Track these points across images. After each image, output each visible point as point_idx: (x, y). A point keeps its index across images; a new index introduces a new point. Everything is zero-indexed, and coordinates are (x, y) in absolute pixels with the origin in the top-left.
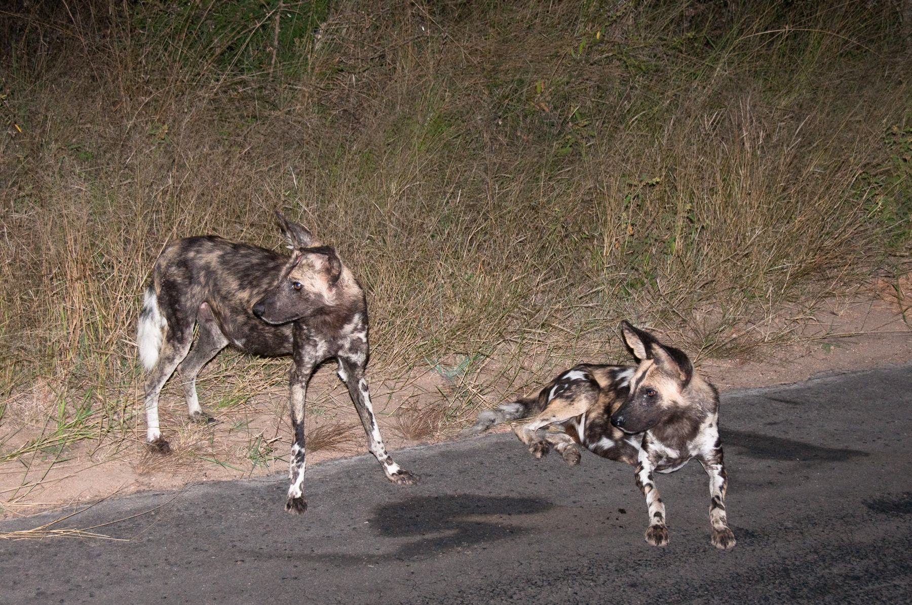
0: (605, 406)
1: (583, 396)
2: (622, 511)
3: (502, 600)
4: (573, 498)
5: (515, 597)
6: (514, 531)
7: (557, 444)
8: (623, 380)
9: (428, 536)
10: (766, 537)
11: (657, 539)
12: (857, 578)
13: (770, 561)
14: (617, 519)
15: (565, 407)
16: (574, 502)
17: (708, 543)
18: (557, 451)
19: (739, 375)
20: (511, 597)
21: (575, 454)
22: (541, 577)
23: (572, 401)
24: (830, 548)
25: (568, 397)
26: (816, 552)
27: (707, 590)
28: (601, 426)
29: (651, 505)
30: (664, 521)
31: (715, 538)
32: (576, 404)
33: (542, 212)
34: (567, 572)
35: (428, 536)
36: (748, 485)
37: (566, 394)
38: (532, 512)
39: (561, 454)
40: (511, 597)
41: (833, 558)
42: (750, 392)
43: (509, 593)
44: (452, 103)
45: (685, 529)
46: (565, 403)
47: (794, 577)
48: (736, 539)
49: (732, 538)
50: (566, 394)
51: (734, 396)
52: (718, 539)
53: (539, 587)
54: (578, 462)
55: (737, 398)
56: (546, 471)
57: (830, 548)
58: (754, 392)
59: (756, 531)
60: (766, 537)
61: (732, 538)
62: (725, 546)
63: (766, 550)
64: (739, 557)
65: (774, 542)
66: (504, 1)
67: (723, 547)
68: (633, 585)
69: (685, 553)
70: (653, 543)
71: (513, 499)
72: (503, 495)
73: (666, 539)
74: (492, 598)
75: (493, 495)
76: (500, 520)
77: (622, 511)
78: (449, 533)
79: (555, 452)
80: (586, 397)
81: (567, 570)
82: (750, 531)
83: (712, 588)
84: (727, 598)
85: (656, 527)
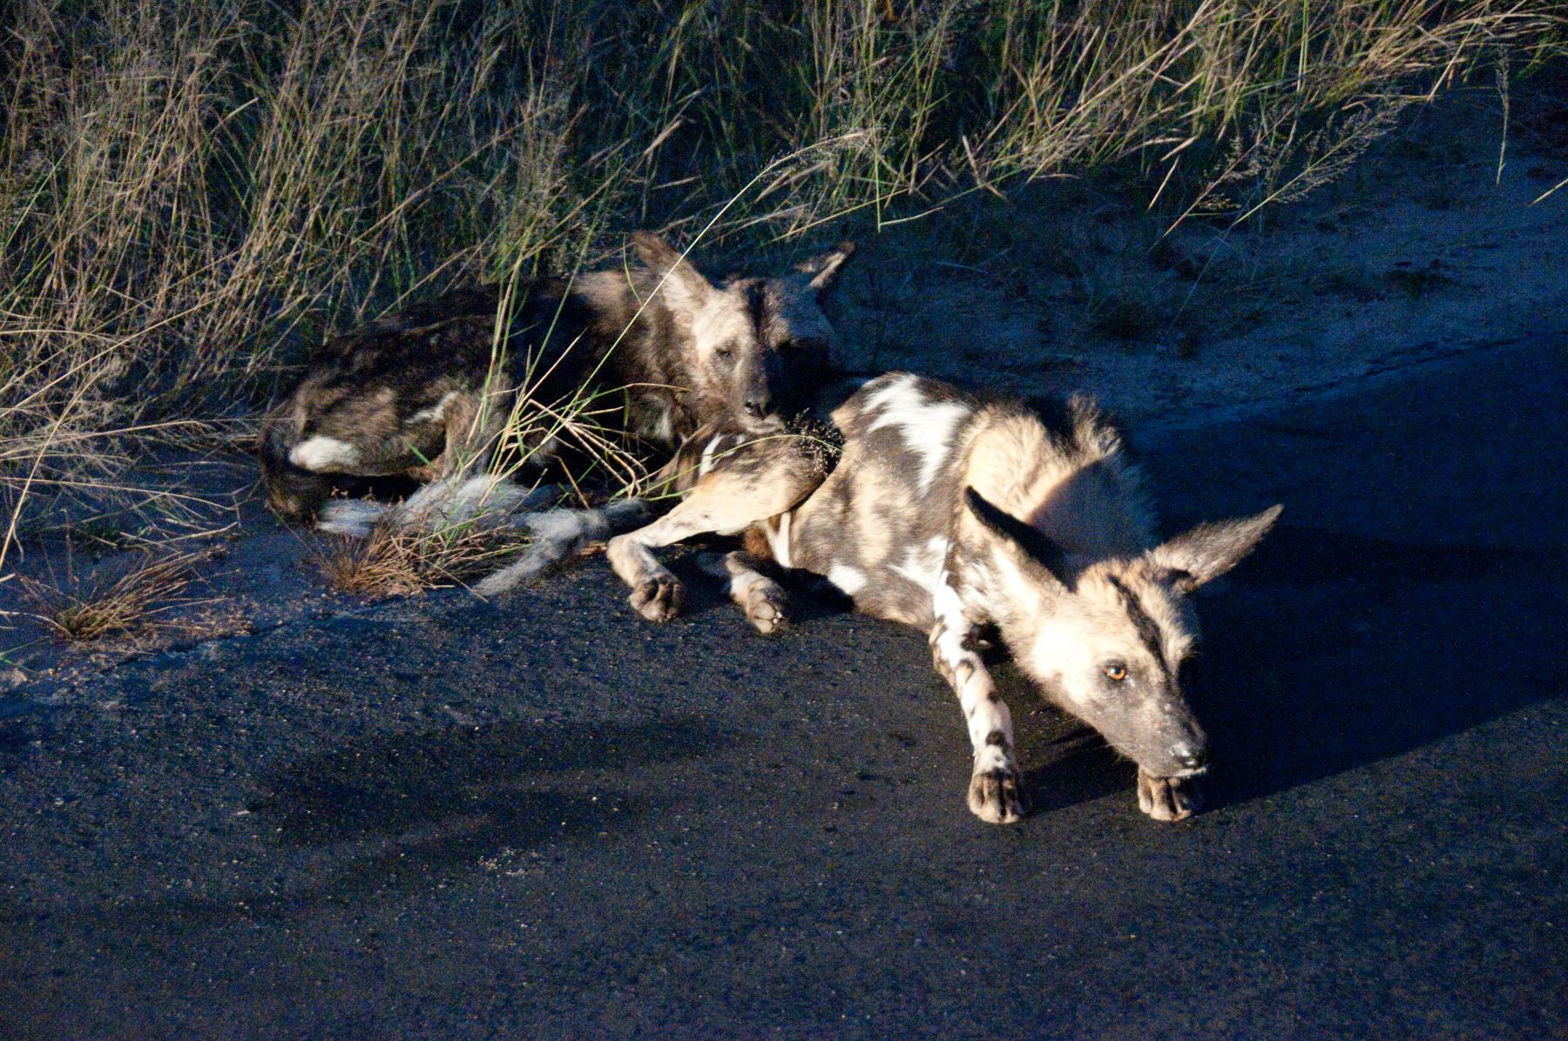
2: (908, 742)
3: (611, 989)
5: (645, 979)
6: (630, 810)
8: (880, 411)
9: (411, 838)
12: (1522, 876)
20: (634, 981)
22: (707, 924)
23: (754, 480)
24: (1449, 801)
26: (1410, 815)
27: (1134, 927)
28: (827, 534)
29: (973, 713)
33: (1149, 1011)
34: (775, 906)
35: (411, 838)
40: (634, 981)
41: (1455, 826)
43: (629, 971)
44: (12, 794)
47: (1356, 880)
53: (705, 948)
57: (1449, 801)
58: (1228, 414)
66: (220, 3)
68: (948, 929)
74: (585, 984)
77: (908, 742)
78: (462, 825)
80: (790, 473)
81: (777, 900)
83: (1150, 922)
84: (1188, 947)
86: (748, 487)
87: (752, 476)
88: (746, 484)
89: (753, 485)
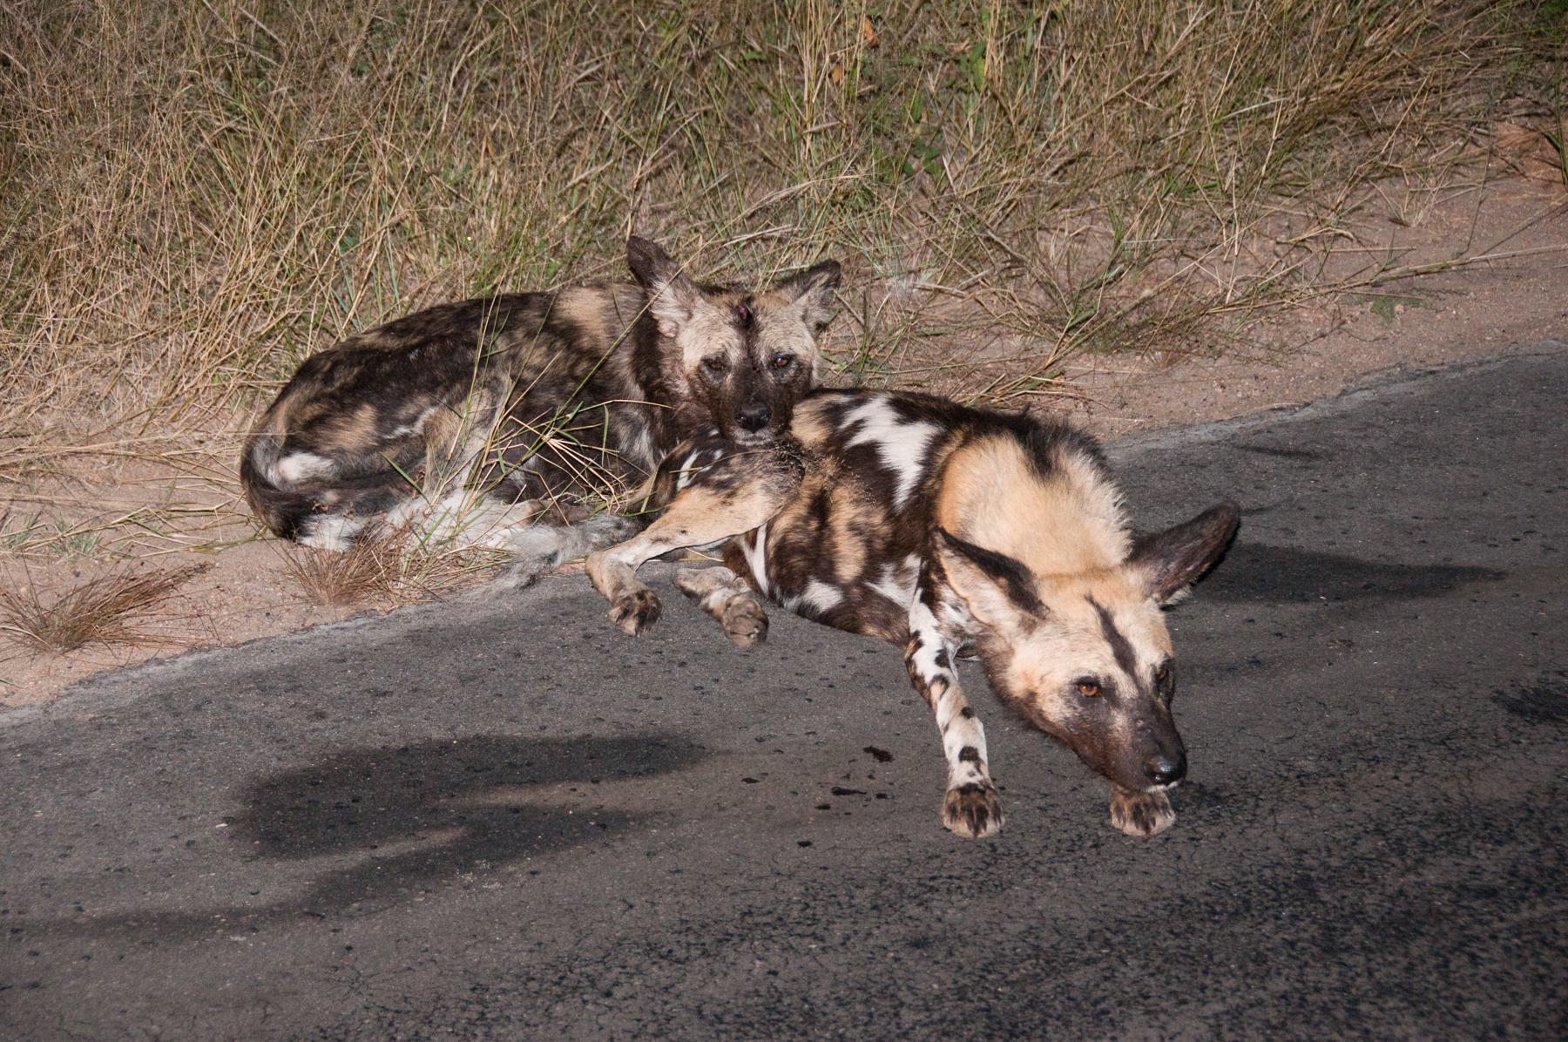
0: (811, 497)
1: (757, 484)
4: (755, 731)
7: (708, 594)
10: (1251, 801)
11: (971, 815)
13: (1264, 862)
14: (871, 777)
15: (711, 509)
16: (760, 740)
17: (1102, 824)
18: (709, 611)
19: (1164, 392)
21: (754, 616)
23: (729, 496)
25: (721, 485)
30: (985, 774)
31: (1119, 810)
32: (739, 505)
36: (1198, 671)
37: (716, 477)
38: (651, 772)
39: (719, 620)
42: (1192, 435)
45: (1044, 790)
46: (715, 500)
48: (1176, 810)
49: (1164, 807)
50: (716, 477)
51: (1153, 446)
52: (1127, 812)
54: (762, 637)
55: (1161, 452)
56: (682, 664)
58: (1204, 434)
59: (1226, 787)
60: (1251, 801)
61: (1164, 807)
62: (1147, 828)
63: (1252, 833)
64: (1184, 855)
65: (1272, 811)
67: (1140, 833)
69: (1048, 854)
70: (962, 828)
71: (603, 743)
72: (576, 733)
73: (997, 817)
75: (549, 733)
76: (573, 798)
77: (883, 756)
79: (704, 615)
80: (768, 489)
82: (1210, 788)
85: (966, 790)
86: (724, 502)
87: (729, 491)
88: (722, 499)
89: (729, 500)
